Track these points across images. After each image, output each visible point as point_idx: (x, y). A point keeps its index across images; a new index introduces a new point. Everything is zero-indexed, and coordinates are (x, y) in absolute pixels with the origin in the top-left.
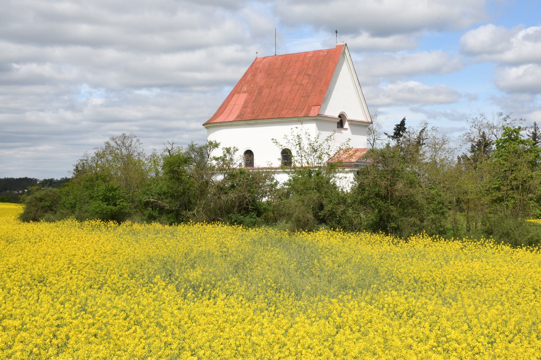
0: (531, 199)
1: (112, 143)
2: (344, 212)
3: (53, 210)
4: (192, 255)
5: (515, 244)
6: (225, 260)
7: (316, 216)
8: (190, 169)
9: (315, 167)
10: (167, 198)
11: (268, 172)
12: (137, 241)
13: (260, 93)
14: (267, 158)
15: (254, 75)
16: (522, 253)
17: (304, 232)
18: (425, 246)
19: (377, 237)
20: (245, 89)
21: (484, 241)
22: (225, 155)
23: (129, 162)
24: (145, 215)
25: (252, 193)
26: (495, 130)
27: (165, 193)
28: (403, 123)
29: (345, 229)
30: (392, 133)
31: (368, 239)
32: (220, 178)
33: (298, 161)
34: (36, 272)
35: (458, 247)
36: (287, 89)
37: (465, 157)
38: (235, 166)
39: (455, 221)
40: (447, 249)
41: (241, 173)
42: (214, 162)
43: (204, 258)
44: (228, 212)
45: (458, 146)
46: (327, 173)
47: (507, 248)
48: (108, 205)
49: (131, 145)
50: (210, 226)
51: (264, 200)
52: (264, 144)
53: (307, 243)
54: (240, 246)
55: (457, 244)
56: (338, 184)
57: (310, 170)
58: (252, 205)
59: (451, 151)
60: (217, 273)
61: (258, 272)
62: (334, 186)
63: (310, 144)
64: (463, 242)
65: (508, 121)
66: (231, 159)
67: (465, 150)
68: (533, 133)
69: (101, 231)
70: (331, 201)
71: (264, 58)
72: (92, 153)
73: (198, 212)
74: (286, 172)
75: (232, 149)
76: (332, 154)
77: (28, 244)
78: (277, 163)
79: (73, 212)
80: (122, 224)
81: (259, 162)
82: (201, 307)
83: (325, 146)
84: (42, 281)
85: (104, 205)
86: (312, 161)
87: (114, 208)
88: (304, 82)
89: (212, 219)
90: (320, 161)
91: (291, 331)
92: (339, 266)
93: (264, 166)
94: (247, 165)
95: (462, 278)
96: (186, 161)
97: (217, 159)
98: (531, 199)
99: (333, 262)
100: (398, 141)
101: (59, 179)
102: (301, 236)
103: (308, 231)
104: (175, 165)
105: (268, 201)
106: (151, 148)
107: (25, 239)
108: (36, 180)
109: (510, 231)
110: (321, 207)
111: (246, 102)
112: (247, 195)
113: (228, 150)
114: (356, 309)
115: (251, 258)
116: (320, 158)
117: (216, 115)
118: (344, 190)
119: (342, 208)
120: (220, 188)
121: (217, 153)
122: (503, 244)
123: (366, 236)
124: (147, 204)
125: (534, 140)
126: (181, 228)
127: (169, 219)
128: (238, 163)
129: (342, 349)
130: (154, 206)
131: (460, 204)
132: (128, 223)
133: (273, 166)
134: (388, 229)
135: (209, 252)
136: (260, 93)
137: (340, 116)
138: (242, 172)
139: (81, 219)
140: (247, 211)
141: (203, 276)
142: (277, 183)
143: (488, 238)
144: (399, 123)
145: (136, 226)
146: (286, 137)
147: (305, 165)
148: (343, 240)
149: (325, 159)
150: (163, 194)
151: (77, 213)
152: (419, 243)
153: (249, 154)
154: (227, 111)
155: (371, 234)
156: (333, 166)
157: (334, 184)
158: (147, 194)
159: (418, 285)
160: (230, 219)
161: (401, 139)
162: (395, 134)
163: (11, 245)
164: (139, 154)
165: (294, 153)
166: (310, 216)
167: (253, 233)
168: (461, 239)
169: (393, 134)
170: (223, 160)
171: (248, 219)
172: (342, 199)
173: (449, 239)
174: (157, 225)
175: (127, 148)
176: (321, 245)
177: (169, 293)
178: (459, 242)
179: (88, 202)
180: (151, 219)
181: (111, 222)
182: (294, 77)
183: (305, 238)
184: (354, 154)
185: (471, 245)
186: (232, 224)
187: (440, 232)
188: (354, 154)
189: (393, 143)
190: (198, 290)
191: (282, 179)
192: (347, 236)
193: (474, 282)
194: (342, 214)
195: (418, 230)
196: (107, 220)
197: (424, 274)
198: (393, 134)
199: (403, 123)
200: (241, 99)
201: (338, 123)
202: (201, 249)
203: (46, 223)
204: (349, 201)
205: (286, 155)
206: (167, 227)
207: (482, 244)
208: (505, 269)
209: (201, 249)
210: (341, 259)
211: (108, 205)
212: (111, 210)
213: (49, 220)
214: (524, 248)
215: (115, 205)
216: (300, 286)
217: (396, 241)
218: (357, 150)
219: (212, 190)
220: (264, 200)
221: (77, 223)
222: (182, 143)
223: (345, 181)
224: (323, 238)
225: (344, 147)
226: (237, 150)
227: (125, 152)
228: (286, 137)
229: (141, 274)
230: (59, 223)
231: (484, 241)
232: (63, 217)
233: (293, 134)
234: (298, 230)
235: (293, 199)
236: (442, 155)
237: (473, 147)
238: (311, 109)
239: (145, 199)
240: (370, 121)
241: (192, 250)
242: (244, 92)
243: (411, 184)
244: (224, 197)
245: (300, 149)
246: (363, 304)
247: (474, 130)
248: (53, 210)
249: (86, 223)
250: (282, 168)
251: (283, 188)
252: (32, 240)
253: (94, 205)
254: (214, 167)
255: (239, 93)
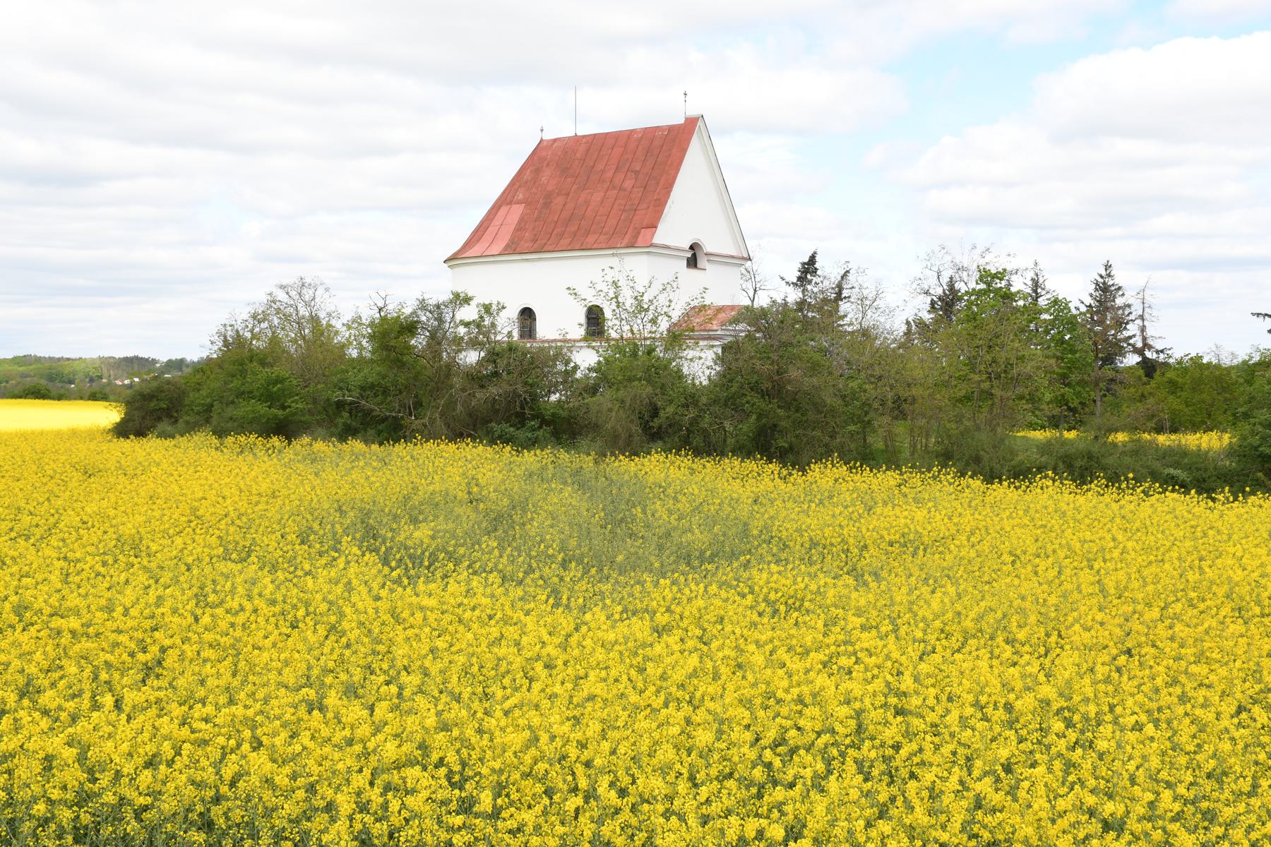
0: (1021, 398)
1: (281, 296)
2: (694, 421)
3: (172, 416)
4: (416, 500)
5: (991, 477)
6: (476, 508)
7: (646, 428)
8: (419, 341)
9: (645, 339)
10: (376, 395)
11: (561, 348)
12: (316, 474)
13: (547, 205)
14: (560, 323)
15: (538, 171)
16: (1002, 492)
17: (621, 457)
18: (836, 480)
19: (751, 465)
20: (521, 196)
21: (939, 471)
22: (481, 317)
23: (318, 331)
24: (336, 426)
25: (531, 386)
26: (965, 274)
27: (372, 386)
28: (812, 260)
29: (698, 453)
30: (793, 275)
31: (737, 469)
32: (471, 357)
33: (614, 328)
34: (128, 530)
35: (893, 482)
36: (598, 196)
37: (921, 323)
38: (499, 338)
39: (890, 437)
40: (873, 487)
41: (510, 349)
42: (462, 330)
43: (437, 504)
44: (486, 421)
45: (901, 303)
46: (666, 350)
47: (977, 483)
48: (270, 407)
49: (314, 299)
50: (452, 447)
51: (554, 398)
52: (554, 296)
53: (626, 477)
54: (503, 481)
55: (889, 478)
56: (685, 370)
57: (635, 345)
58: (532, 409)
59: (890, 312)
60: (459, 532)
61: (532, 528)
62: (679, 375)
63: (636, 298)
64: (901, 474)
65: (989, 258)
66: (493, 325)
67: (920, 308)
68: (1033, 280)
69: (255, 455)
70: (671, 402)
71: (555, 140)
72: (243, 314)
73: (432, 421)
74: (593, 348)
75: (494, 307)
76: (676, 315)
77: (122, 478)
78: (578, 332)
79: (208, 421)
80: (294, 443)
81: (546, 330)
82: (427, 595)
83: (663, 299)
84: (136, 549)
85: (262, 409)
86: (642, 327)
87: (280, 413)
88: (628, 184)
89: (456, 435)
90: (654, 329)
91: (574, 640)
92: (679, 519)
93: (552, 338)
94: (522, 336)
95: (892, 537)
96: (410, 327)
97: (467, 325)
98: (1021, 398)
99: (670, 512)
100: (803, 292)
101: (196, 360)
102: (617, 464)
103: (630, 456)
104: (392, 334)
105: (559, 401)
106: (350, 304)
107: (117, 469)
108: (154, 361)
109: (982, 453)
110: (655, 412)
111: (522, 220)
112: (520, 389)
113: (487, 308)
114: (700, 598)
115: (520, 505)
116: (654, 321)
117: (469, 244)
118: (697, 382)
119: (692, 413)
120: (476, 378)
121: (468, 313)
122: (972, 477)
123: (733, 464)
124: (340, 405)
125: (1035, 291)
126: (400, 449)
127: (379, 433)
128: (505, 332)
129: (660, 671)
130: (354, 408)
131: (899, 408)
132: (306, 440)
133: (569, 337)
134: (772, 450)
135: (447, 494)
136: (547, 205)
137: (692, 248)
138: (511, 348)
139: (221, 433)
140: (520, 420)
141: (433, 538)
142: (576, 368)
143: (945, 466)
144: (806, 260)
145: (320, 446)
146: (593, 285)
147: (627, 335)
148: (692, 472)
149: (664, 325)
150: (368, 389)
151: (215, 421)
152: (825, 476)
153: (527, 314)
154: (488, 236)
155: (742, 461)
156: (676, 338)
157: (680, 371)
158: (341, 389)
159: (815, 550)
160: (489, 432)
161: (809, 287)
162: (799, 279)
163: (92, 479)
164: (329, 315)
165: (608, 314)
166: (636, 429)
167: (531, 459)
168: (898, 467)
169: (795, 280)
170: (478, 326)
171: (522, 434)
172: (691, 397)
173: (879, 468)
174: (356, 445)
175: (307, 304)
176: (651, 479)
177: (364, 569)
178: (895, 474)
179: (233, 402)
180: (345, 434)
181: (275, 439)
182: (609, 174)
183: (625, 467)
184: (715, 315)
185: (916, 479)
186: (492, 442)
187: (866, 458)
188: (715, 315)
189: (794, 296)
190: (415, 565)
191: (586, 359)
192: (698, 463)
193: (908, 544)
194: (691, 424)
195: (824, 454)
196: (268, 436)
197: (827, 532)
198: (795, 280)
199: (812, 260)
200: (517, 211)
201: (688, 260)
202: (431, 488)
203: (158, 440)
204: (704, 400)
205: (594, 318)
206: (375, 447)
207: (934, 478)
208: (968, 521)
209: (431, 488)
210: (684, 505)
211: (270, 407)
212: (275, 417)
213: (164, 435)
214: (1006, 483)
215: (283, 408)
216: (613, 553)
217: (784, 472)
218: (721, 309)
219: (457, 381)
220: (554, 398)
221: (215, 441)
222: (403, 299)
223: (700, 364)
224: (658, 468)
225: (695, 303)
226: (504, 308)
227: (303, 311)
228: (593, 285)
229: (316, 536)
230: (182, 441)
231: (939, 471)
232: (190, 428)
233: (607, 278)
234: (613, 454)
235: (605, 398)
236: (871, 318)
237: (933, 303)
238: (639, 233)
239: (337, 396)
240: (745, 255)
241: (416, 489)
242: (519, 202)
243: (814, 368)
244: (480, 395)
245: (618, 307)
246: (713, 588)
247: (928, 272)
248: (172, 416)
249: (230, 440)
250: (585, 339)
251: (587, 377)
252: (130, 472)
253: (246, 408)
254: (462, 338)
255: (510, 203)
